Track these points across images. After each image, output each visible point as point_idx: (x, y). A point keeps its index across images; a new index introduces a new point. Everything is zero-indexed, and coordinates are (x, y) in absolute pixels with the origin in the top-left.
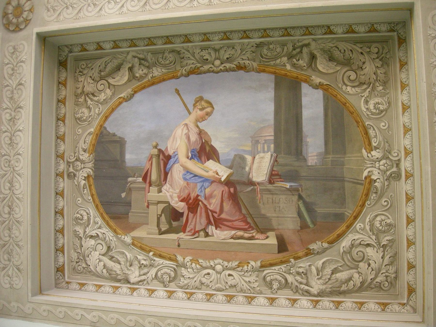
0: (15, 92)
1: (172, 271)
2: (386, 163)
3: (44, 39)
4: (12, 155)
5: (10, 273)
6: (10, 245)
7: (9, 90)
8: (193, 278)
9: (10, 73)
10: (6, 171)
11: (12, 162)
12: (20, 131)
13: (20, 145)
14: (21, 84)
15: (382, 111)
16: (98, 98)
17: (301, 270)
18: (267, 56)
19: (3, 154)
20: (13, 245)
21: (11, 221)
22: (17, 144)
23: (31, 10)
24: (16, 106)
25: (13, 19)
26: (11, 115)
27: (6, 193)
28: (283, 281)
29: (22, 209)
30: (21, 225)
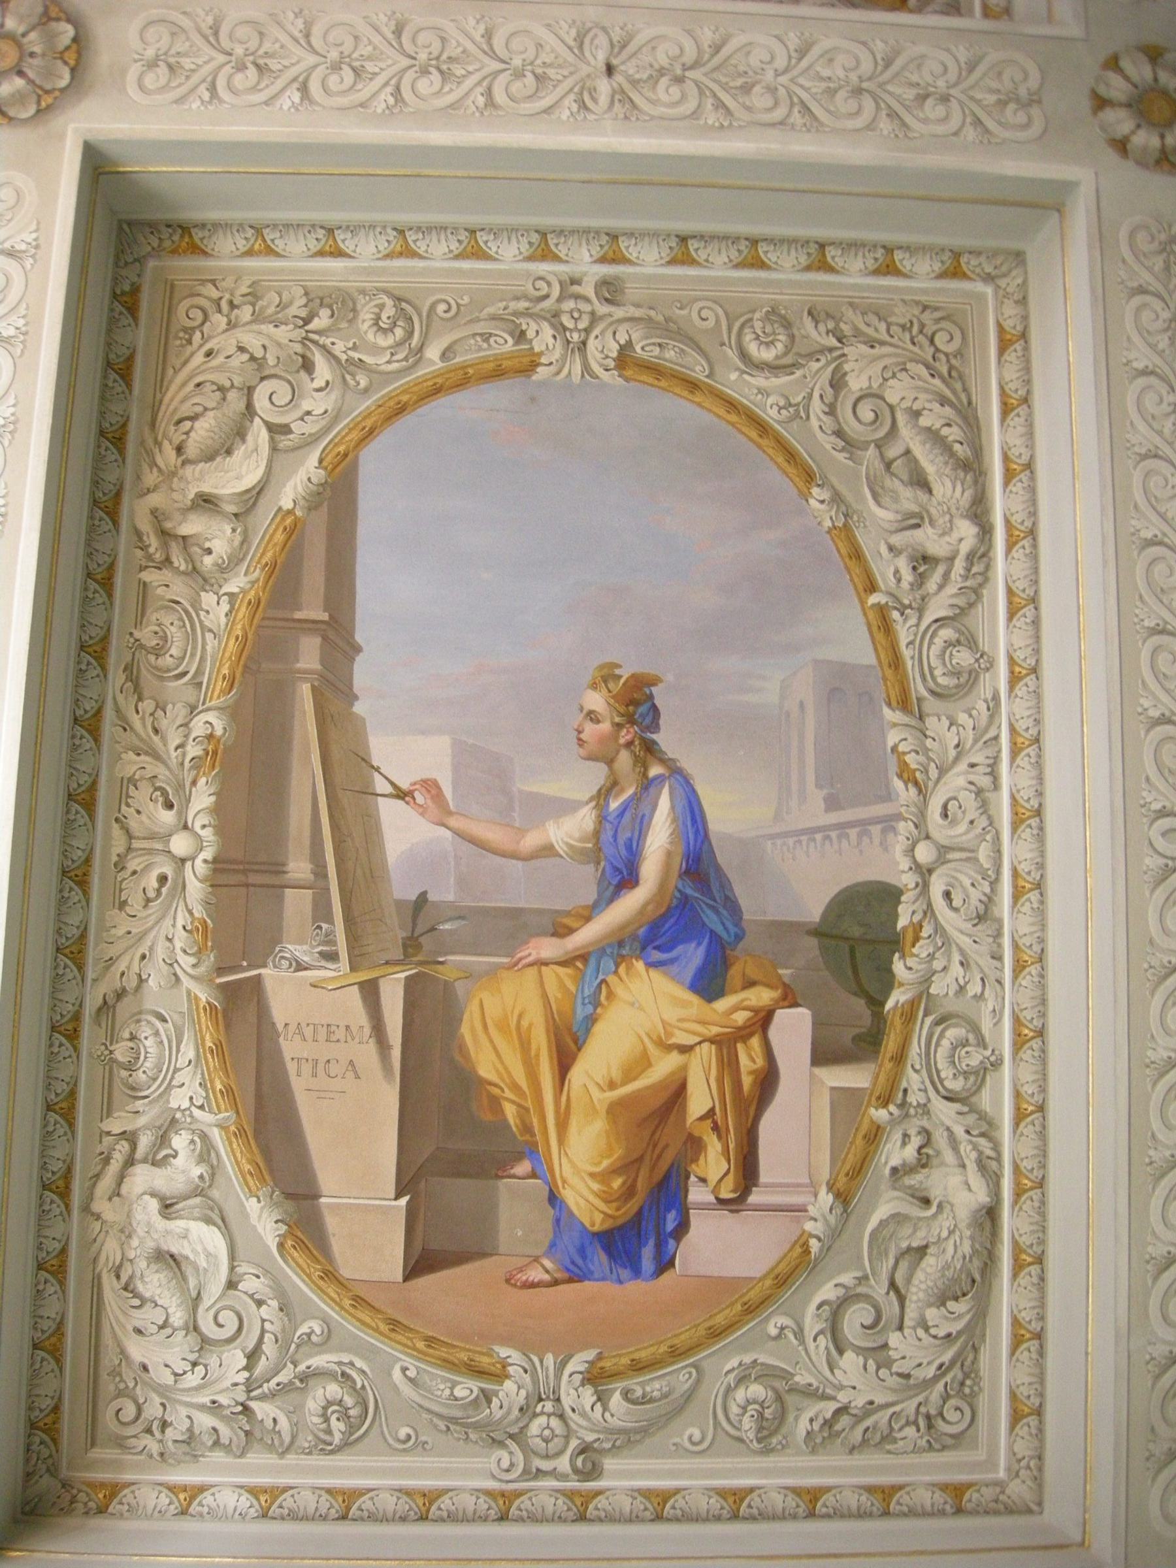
1: (943, 1031)
7: (231, 76)
8: (962, 951)
17: (908, 577)
28: (946, 633)
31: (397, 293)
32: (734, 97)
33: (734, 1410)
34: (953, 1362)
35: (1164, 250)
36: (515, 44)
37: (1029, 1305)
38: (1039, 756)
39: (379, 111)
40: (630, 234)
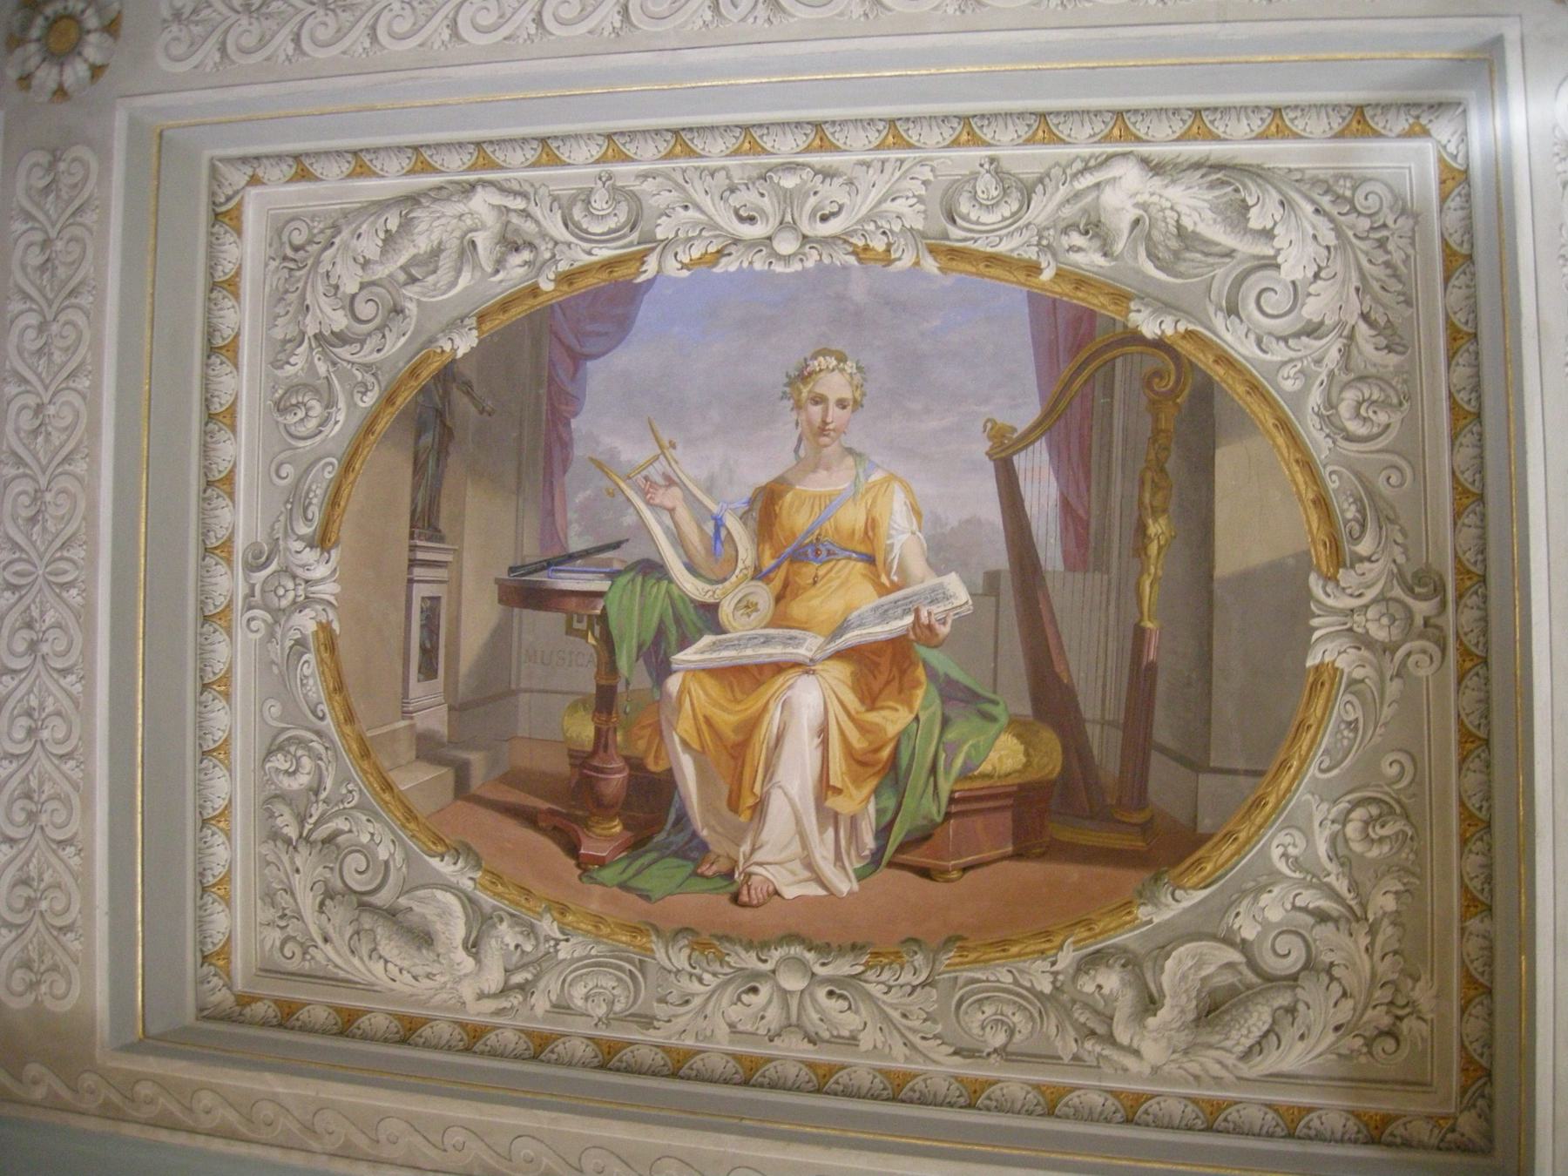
2: (280, 598)
10: (62, 558)
15: (280, 748)
18: (619, 980)
31: (264, 752)
33: (1362, 431)
34: (1313, 202)
35: (333, 10)
37: (1245, 122)
38: (908, 119)
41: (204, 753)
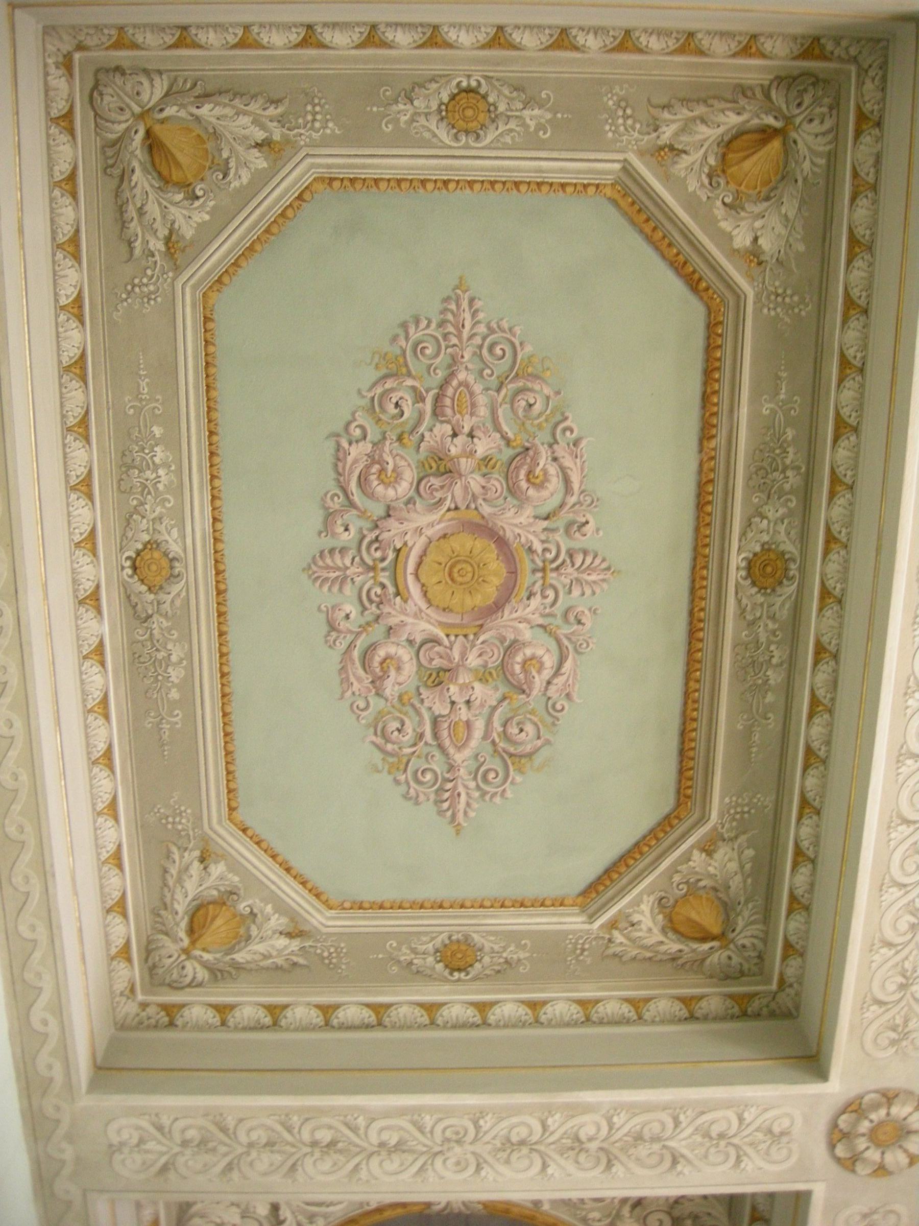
0: (656, 1147)
3: (812, 1061)
4: (478, 1148)
5: (151, 1145)
6: (225, 1145)
7: (663, 1130)
9: (713, 1127)
10: (432, 1132)
11: (458, 1149)
12: (545, 1166)
13: (502, 1168)
14: (675, 1162)
16: (628, 1215)
19: (481, 1122)
20: (225, 1155)
21: (294, 1150)
22: (507, 1162)
23: (881, 1170)
24: (615, 1151)
25: (871, 1121)
26: (591, 1139)
27: (370, 1132)
29: (331, 1178)
30: (285, 1176)
32: (344, 1135)
36: (526, 1162)
39: (490, 1116)
40: (524, 1025)
41: (327, 1024)
